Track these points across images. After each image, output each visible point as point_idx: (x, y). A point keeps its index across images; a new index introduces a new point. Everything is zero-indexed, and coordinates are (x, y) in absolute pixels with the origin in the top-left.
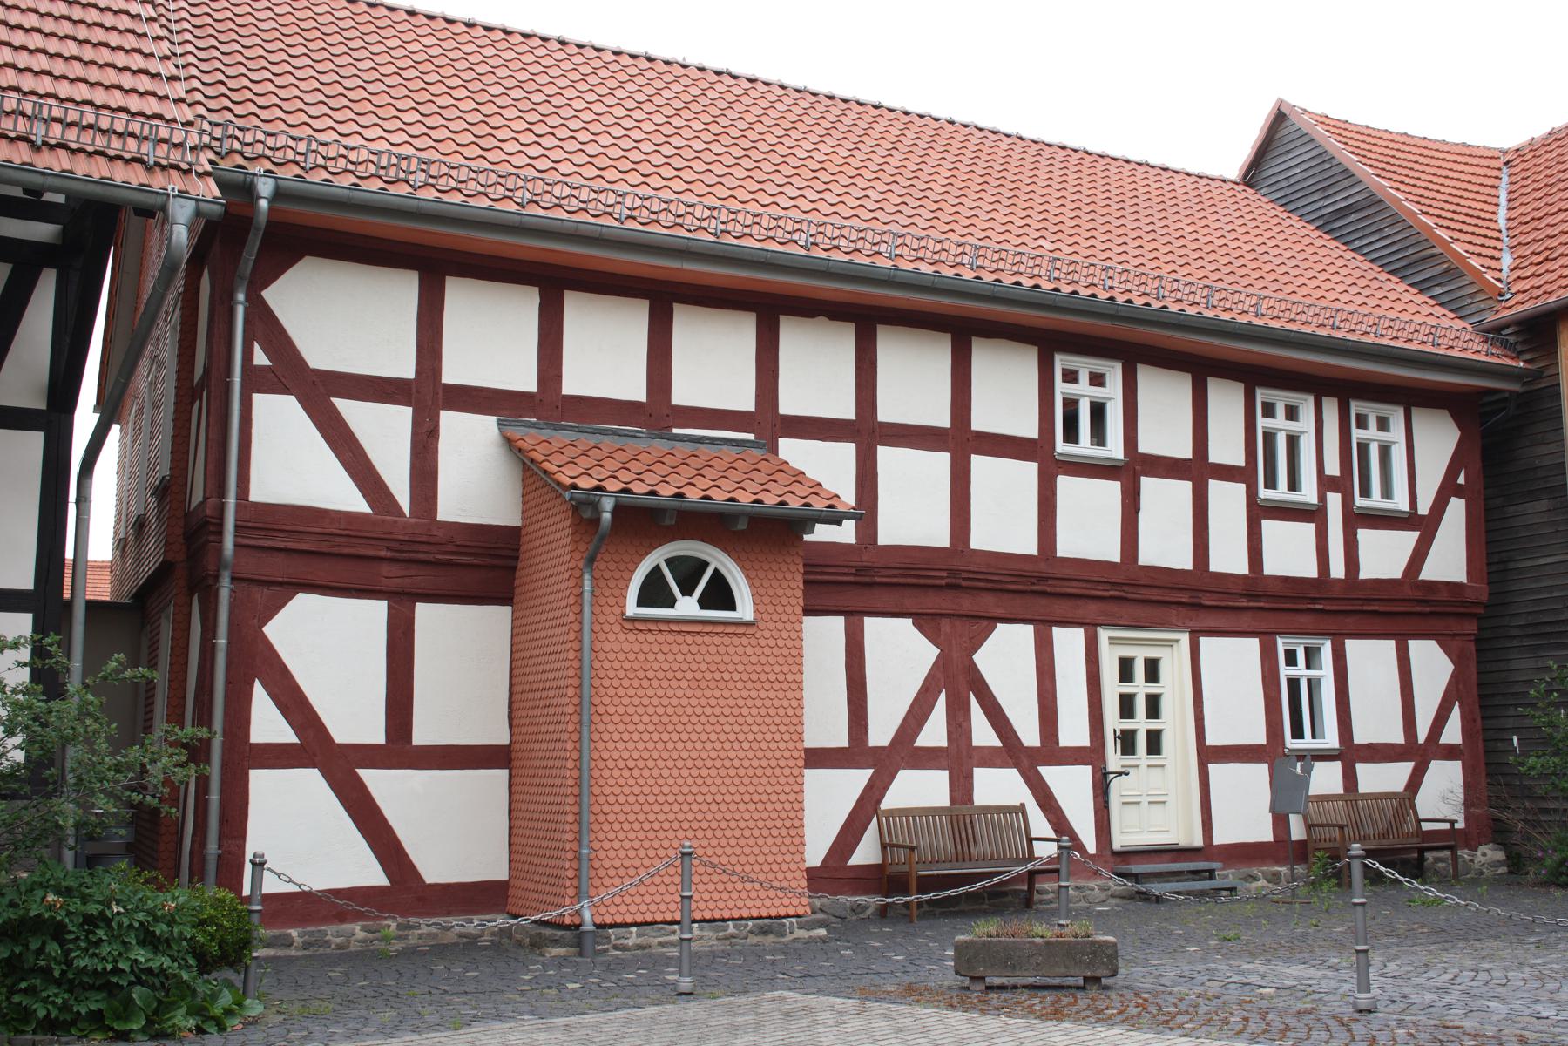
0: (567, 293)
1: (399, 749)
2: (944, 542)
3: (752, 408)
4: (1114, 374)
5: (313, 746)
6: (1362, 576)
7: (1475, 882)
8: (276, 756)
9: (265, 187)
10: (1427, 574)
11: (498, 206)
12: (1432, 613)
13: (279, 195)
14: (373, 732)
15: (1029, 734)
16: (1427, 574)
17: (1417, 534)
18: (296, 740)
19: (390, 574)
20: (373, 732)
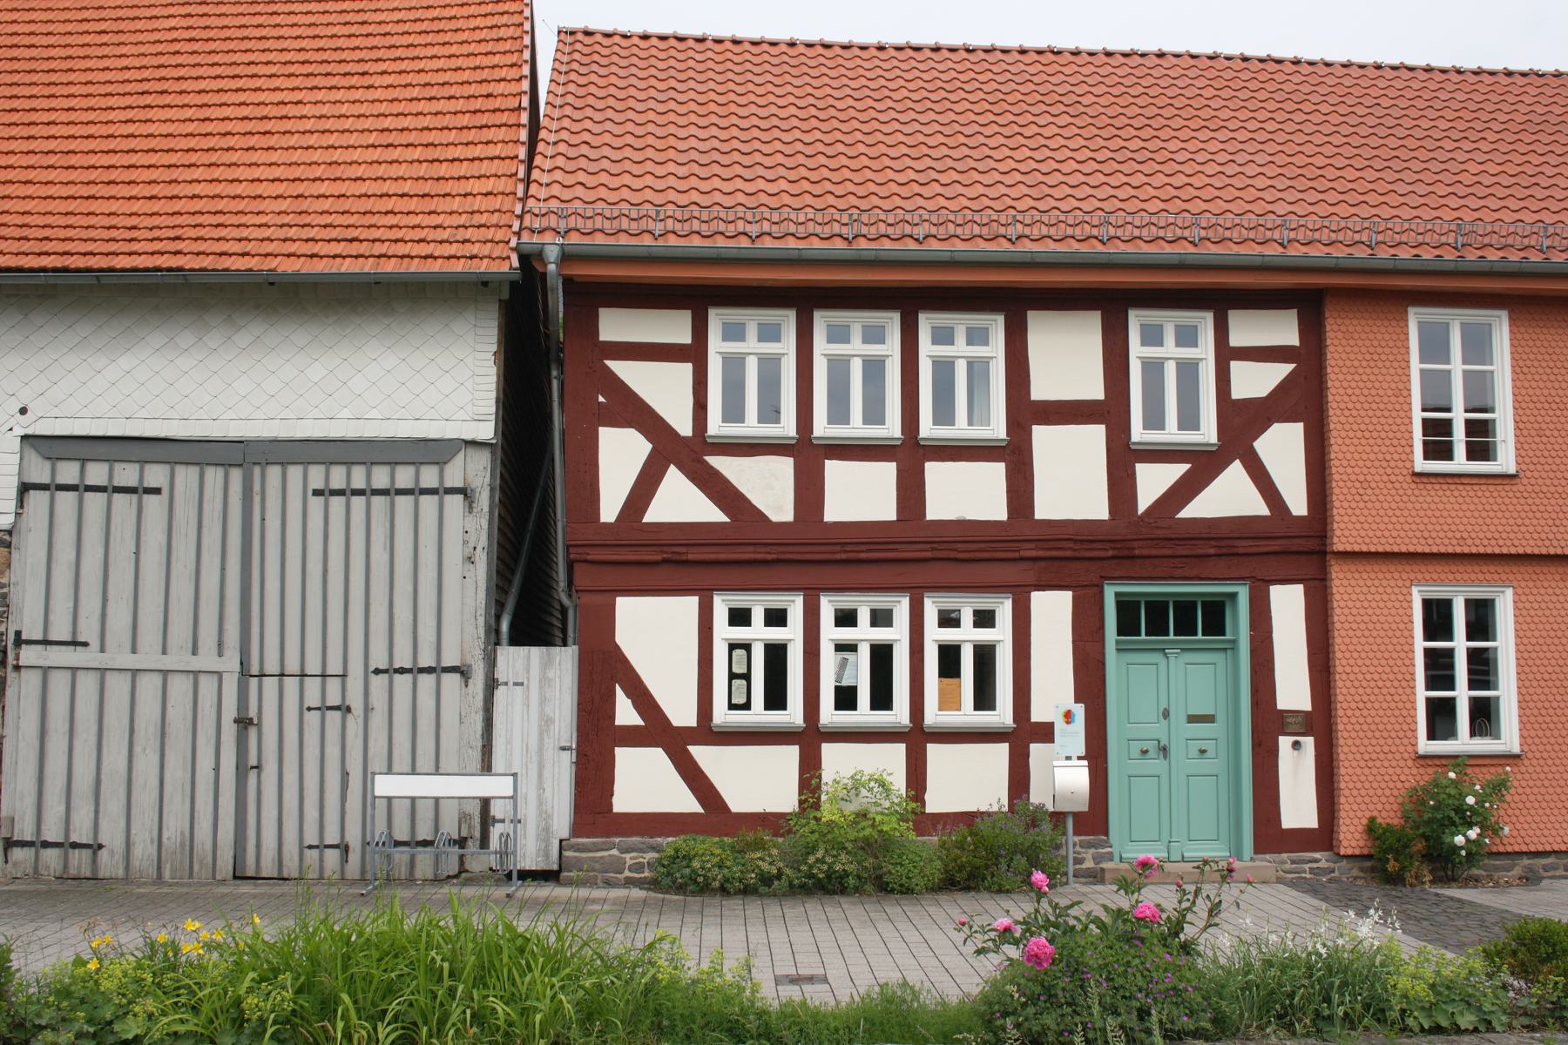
0: (1231, 313)
1: (707, 733)
2: (1001, 514)
3: (1101, 396)
4: (892, 322)
5: (656, 730)
6: (831, 515)
7: (892, 891)
8: (633, 737)
9: (552, 253)
10: (653, 515)
11: (661, 242)
12: (665, 561)
13: (566, 257)
14: (691, 721)
15: (682, 713)
16: (653, 515)
17: (672, 470)
18: (640, 722)
19: (1011, 573)
20: (691, 721)
